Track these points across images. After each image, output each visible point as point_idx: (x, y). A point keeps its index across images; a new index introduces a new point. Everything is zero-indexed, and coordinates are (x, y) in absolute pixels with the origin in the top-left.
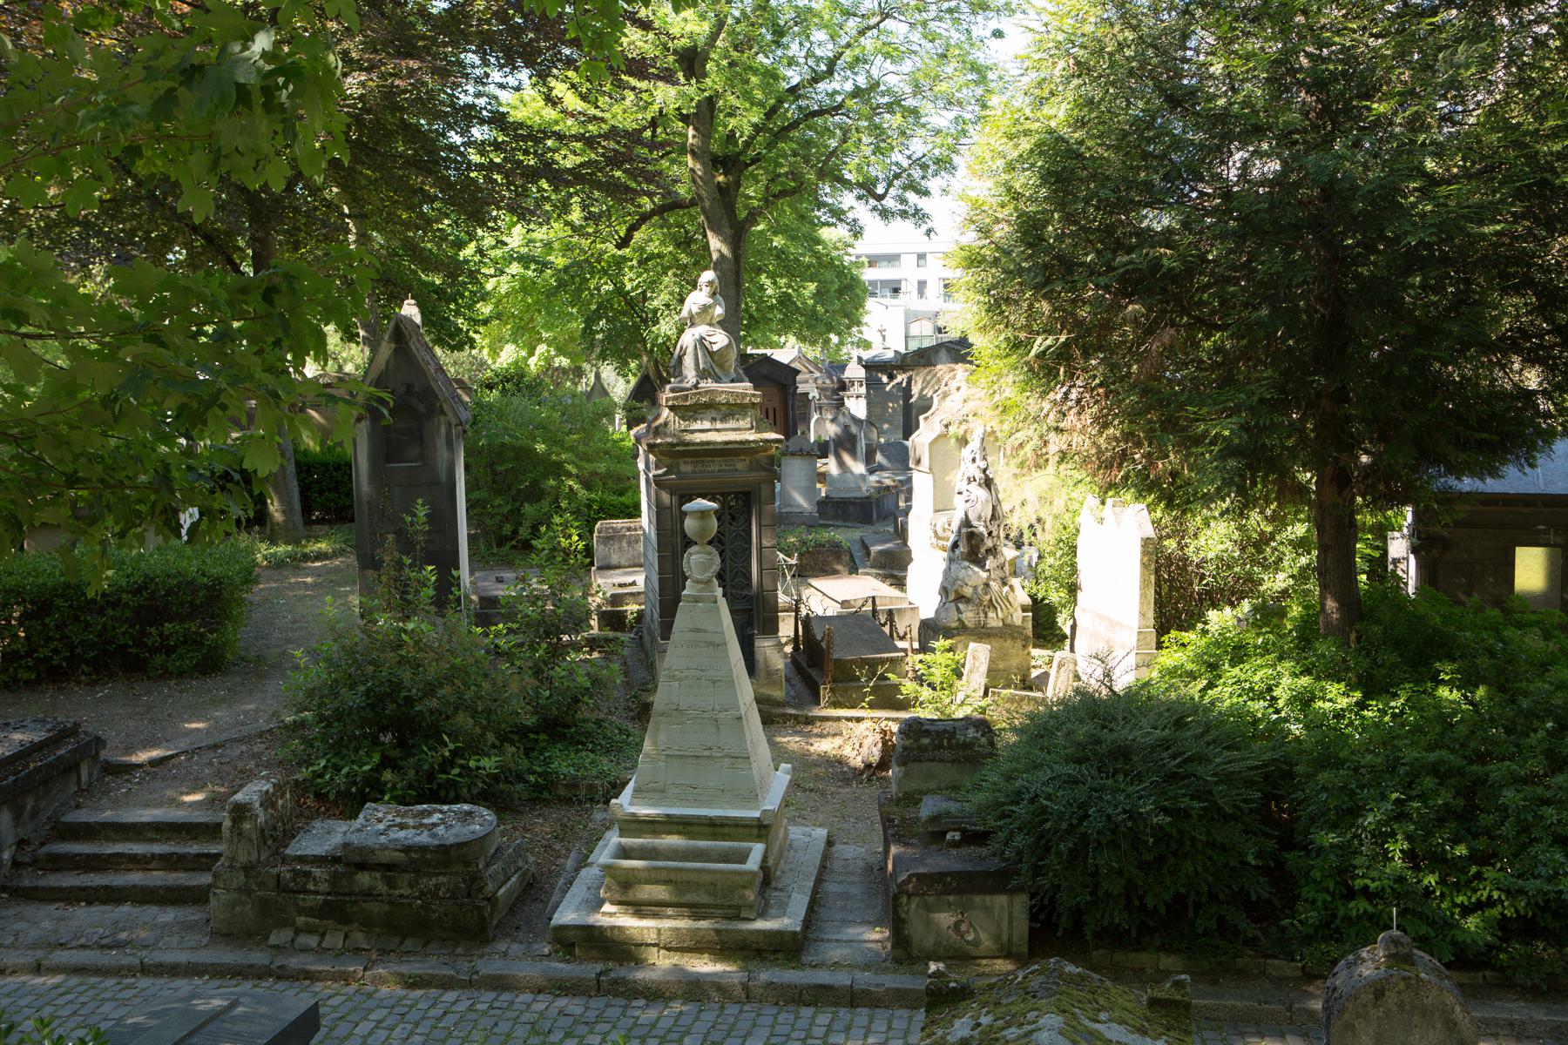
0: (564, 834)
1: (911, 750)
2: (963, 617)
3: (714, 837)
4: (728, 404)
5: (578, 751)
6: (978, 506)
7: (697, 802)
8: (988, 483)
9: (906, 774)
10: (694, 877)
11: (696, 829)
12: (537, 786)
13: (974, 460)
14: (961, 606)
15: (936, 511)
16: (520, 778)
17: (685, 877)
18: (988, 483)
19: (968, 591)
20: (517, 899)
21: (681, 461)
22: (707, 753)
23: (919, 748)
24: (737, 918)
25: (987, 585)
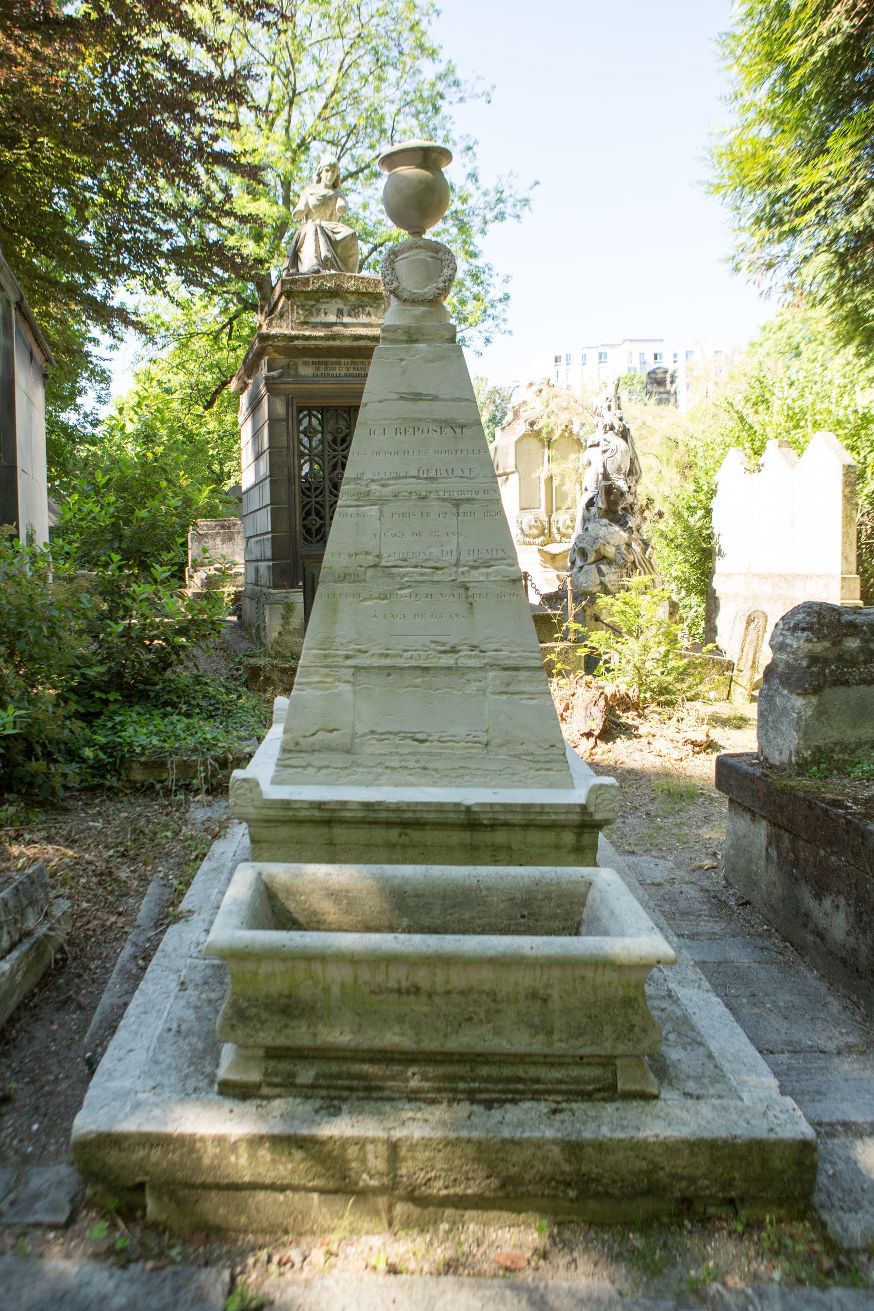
0: (137, 848)
1: (826, 662)
2: (606, 580)
3: (472, 855)
4: (357, 292)
5: (165, 715)
6: (618, 456)
7: (425, 772)
8: (625, 434)
9: (821, 712)
10: (485, 977)
11: (431, 836)
12: (99, 768)
13: (609, 408)
14: (604, 568)
15: (522, 509)
16: (73, 755)
17: (458, 979)
18: (625, 434)
19: (610, 551)
20: (22, 1006)
21: (300, 361)
22: (447, 660)
23: (840, 658)
24: (609, 1092)
25: (629, 545)
